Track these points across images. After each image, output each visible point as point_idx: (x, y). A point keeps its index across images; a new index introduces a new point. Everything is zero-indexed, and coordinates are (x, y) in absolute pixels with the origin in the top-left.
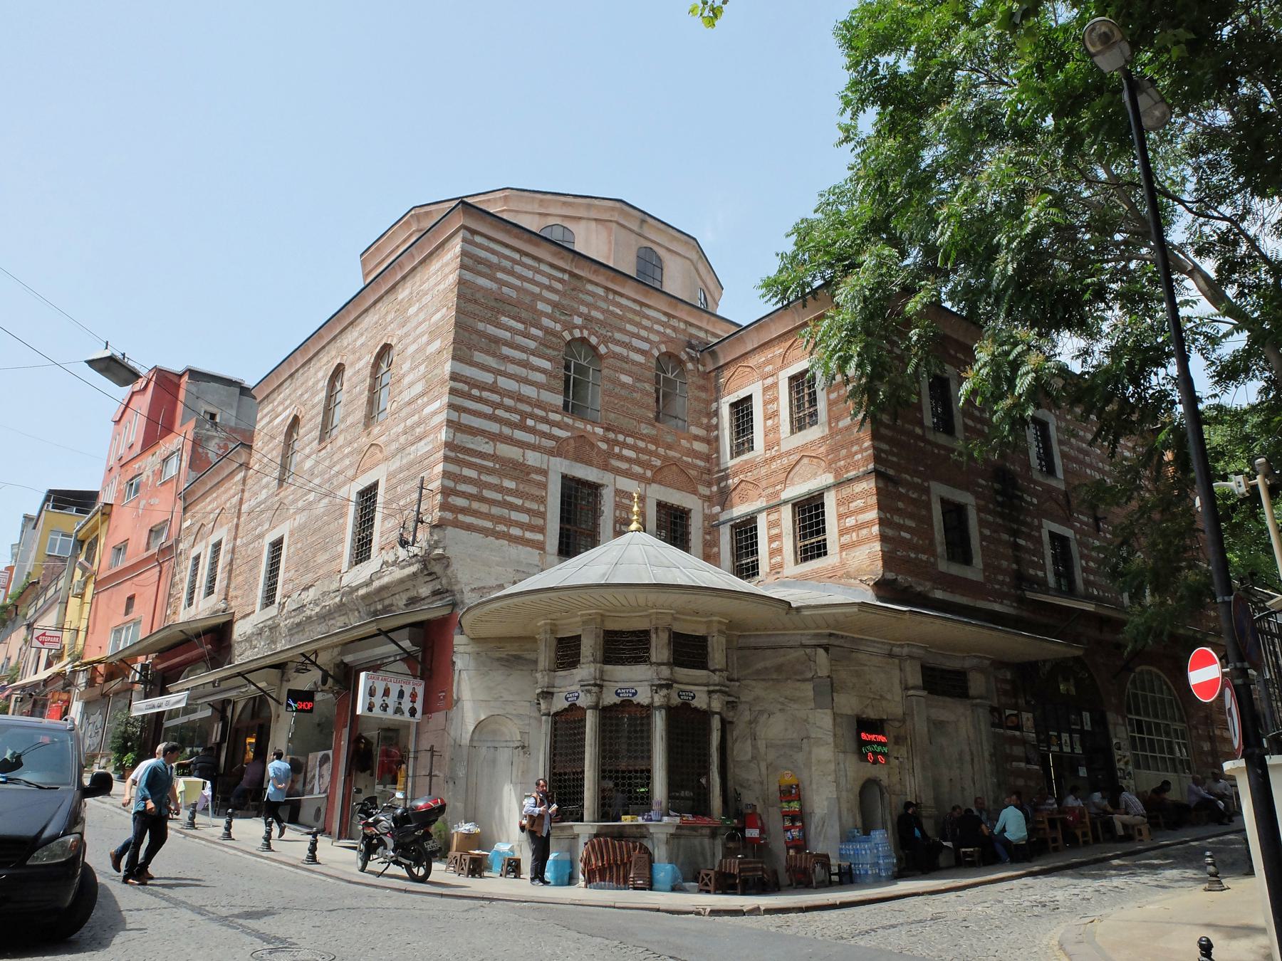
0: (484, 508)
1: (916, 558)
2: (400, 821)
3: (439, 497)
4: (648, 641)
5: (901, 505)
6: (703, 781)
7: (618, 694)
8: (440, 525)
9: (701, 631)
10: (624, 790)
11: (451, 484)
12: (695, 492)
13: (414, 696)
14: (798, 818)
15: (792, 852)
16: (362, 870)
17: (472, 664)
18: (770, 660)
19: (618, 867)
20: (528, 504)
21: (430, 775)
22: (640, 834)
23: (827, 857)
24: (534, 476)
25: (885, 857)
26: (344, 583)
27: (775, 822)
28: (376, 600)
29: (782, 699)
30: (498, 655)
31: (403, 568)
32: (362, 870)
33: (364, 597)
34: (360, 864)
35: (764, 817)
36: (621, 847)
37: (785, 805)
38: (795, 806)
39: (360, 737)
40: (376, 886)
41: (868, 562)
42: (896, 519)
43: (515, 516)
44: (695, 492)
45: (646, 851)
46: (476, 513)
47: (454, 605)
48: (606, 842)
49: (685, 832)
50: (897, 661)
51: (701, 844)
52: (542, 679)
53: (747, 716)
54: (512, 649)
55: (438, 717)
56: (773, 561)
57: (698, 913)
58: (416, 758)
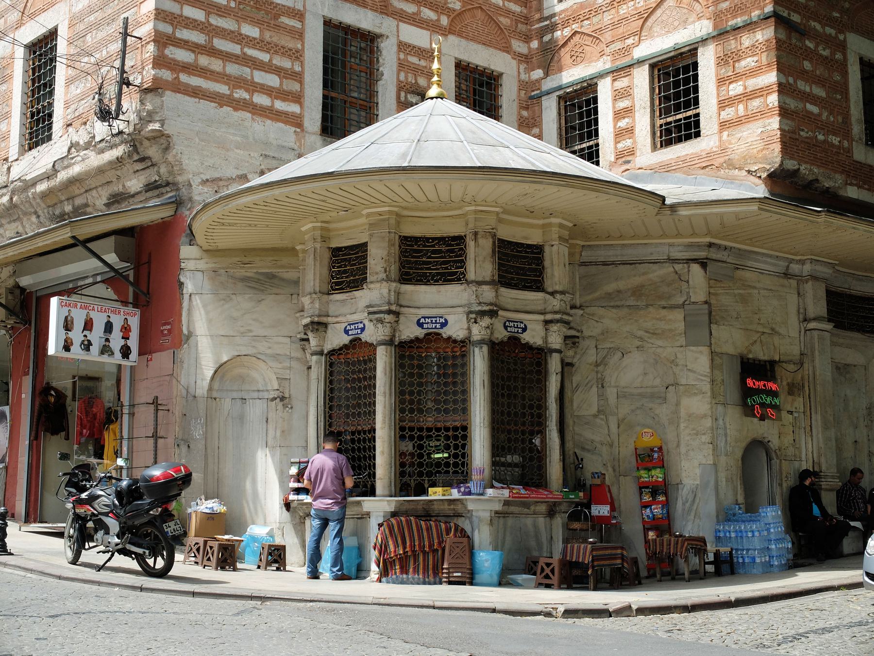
0: (216, 65)
1: (825, 141)
2: (128, 496)
3: (151, 47)
4: (462, 252)
5: (807, 65)
6: (537, 441)
7: (420, 325)
8: (153, 89)
9: (534, 238)
10: (431, 456)
11: (169, 29)
12: (507, 49)
13: (126, 331)
14: (660, 490)
15: (651, 535)
16: (74, 562)
17: (207, 285)
18: (628, 280)
19: (425, 553)
20: (278, 61)
21: (155, 436)
22: (453, 513)
23: (703, 540)
24: (285, 20)
25: (777, 540)
26: (15, 173)
27: (627, 494)
28: (62, 199)
29: (640, 333)
30: (242, 273)
31: (102, 151)
32: (74, 562)
33: (44, 195)
34: (70, 555)
35: (614, 490)
36: (429, 529)
37: (643, 473)
38: (657, 475)
39: (48, 388)
40: (99, 583)
41: (760, 146)
42: (802, 85)
43: (260, 77)
44: (507, 49)
45: (463, 533)
46: (204, 73)
47: (178, 203)
48: (409, 523)
49: (512, 509)
50: (793, 282)
51: (535, 526)
52: (311, 305)
53: (592, 356)
54: (263, 266)
55: (161, 359)
56: (620, 146)
57: (548, 614)
58: (132, 415)
